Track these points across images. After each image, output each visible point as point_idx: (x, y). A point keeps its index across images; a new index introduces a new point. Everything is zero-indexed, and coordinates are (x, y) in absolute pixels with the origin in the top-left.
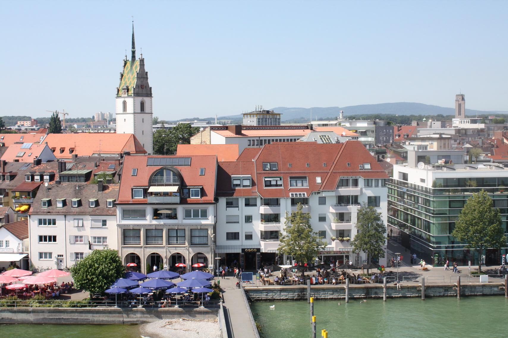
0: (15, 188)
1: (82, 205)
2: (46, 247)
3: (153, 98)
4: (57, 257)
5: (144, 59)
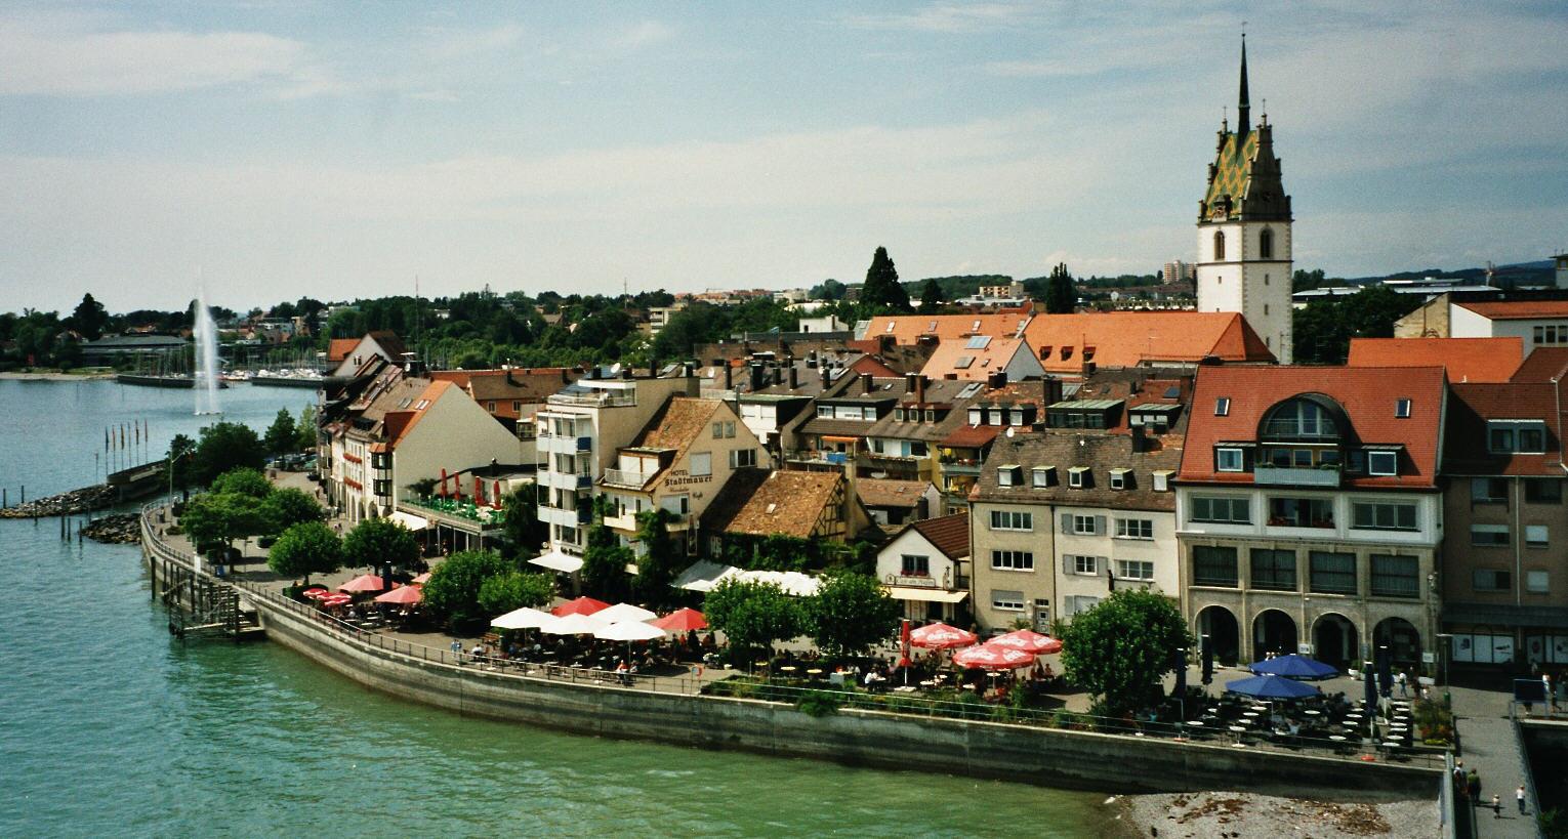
0: (945, 439)
1: (1094, 486)
2: (1009, 578)
3: (1293, 224)
4: (1033, 603)
5: (1270, 126)
